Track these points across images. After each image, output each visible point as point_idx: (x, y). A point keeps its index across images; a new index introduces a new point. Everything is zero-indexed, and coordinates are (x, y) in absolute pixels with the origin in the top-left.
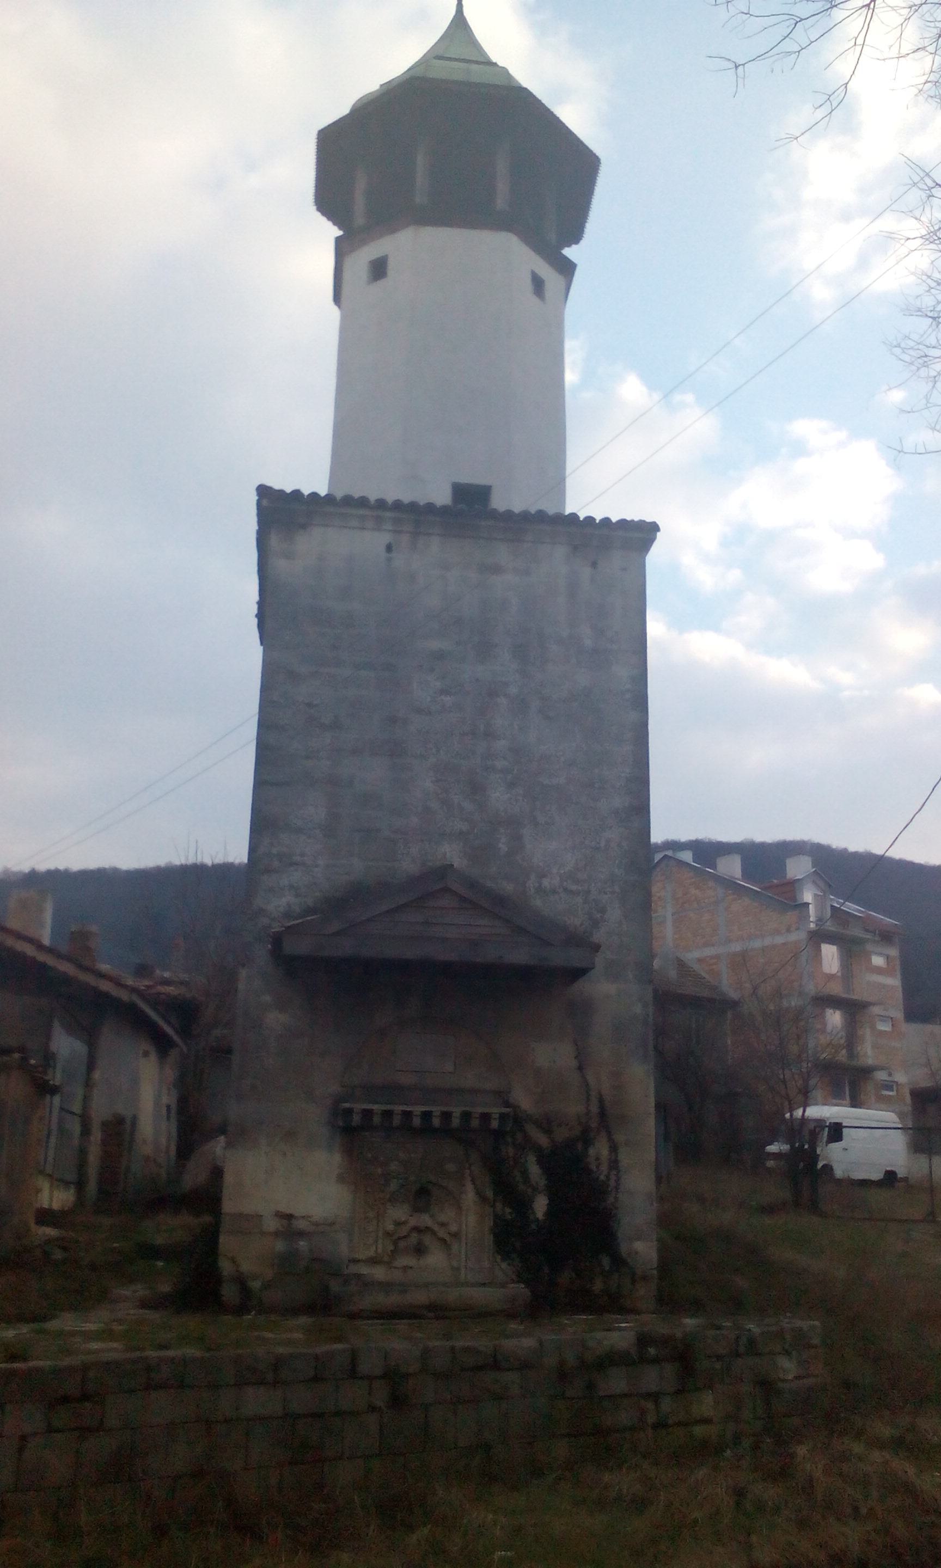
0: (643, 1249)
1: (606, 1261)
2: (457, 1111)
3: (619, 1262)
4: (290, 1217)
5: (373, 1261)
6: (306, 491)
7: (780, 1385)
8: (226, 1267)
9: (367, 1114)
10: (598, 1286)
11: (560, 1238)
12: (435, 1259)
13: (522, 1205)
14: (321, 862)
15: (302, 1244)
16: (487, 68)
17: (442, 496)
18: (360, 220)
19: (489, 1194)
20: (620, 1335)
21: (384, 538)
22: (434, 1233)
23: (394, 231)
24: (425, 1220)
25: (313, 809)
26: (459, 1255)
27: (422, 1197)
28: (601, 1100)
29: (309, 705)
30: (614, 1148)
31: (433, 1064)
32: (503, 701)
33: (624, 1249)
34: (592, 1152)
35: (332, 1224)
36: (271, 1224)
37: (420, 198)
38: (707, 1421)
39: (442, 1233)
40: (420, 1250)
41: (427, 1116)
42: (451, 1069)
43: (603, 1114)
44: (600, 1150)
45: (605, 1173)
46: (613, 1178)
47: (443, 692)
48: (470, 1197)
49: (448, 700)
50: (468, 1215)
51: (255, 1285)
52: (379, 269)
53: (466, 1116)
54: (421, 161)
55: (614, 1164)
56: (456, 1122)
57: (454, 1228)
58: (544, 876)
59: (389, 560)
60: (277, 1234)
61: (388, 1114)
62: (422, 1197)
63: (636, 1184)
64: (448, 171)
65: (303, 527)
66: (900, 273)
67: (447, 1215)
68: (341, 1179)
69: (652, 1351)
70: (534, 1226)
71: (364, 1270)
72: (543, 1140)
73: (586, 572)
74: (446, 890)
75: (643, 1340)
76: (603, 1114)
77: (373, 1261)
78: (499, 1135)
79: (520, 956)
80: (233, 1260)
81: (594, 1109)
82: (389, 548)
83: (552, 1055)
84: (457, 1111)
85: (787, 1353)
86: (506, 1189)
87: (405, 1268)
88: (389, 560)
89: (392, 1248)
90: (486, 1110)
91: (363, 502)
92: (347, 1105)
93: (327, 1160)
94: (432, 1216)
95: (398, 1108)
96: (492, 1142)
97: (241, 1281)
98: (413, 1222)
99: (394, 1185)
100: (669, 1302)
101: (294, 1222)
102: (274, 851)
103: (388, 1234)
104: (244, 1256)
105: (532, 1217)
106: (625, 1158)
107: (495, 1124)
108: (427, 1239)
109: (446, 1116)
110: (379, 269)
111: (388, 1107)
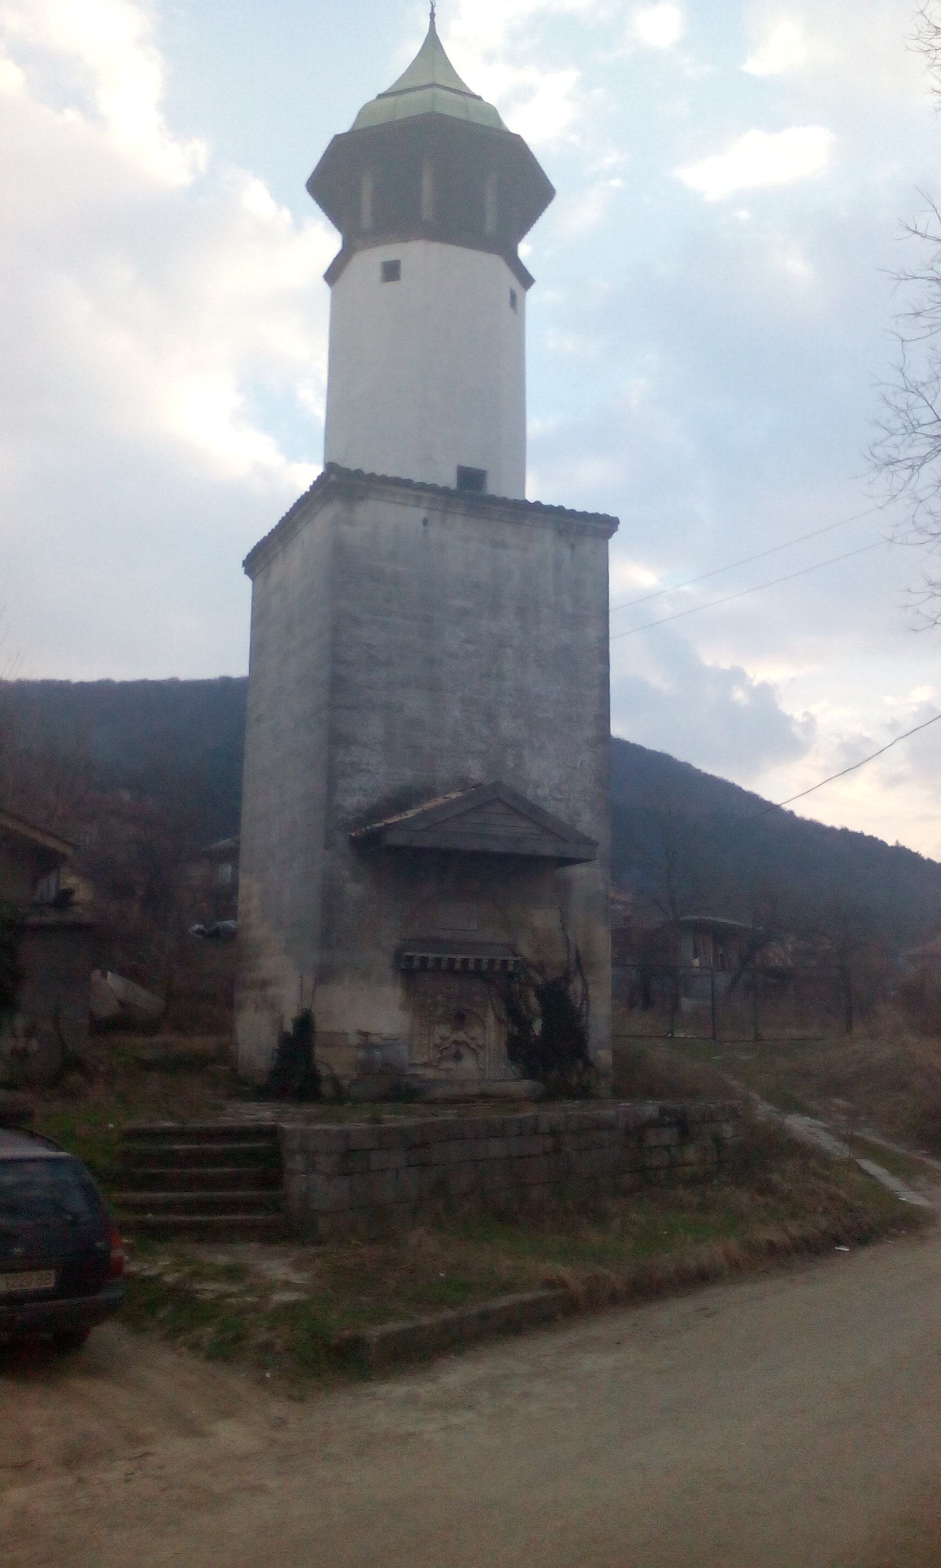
0: (603, 1056)
1: (580, 1064)
2: (485, 959)
3: (588, 1064)
4: (366, 1034)
5: (425, 1065)
6: (568, 508)
7: (725, 1141)
8: (324, 1071)
9: (424, 960)
10: (574, 1080)
11: (551, 1046)
12: (468, 1063)
13: (523, 1023)
14: (381, 770)
15: (377, 1053)
16: (459, 98)
17: (448, 479)
18: (367, 222)
19: (504, 1017)
20: (650, 1109)
21: (422, 513)
22: (468, 1046)
23: (406, 240)
24: (461, 1036)
25: (374, 729)
26: (482, 1060)
27: (460, 1019)
28: (577, 952)
29: (370, 646)
30: (586, 985)
31: (464, 924)
32: (509, 651)
33: (591, 1057)
34: (571, 988)
35: (396, 1039)
36: (354, 1040)
37: (427, 213)
38: (690, 1164)
39: (473, 1045)
40: (458, 1057)
41: (465, 962)
42: (475, 927)
43: (578, 959)
44: (576, 986)
45: (580, 1002)
46: (584, 1007)
47: (467, 641)
48: (491, 1019)
49: (470, 647)
50: (490, 1034)
51: (345, 1082)
52: (391, 271)
53: (492, 962)
54: (427, 183)
55: (586, 996)
56: (484, 967)
57: (481, 1042)
58: (539, 787)
59: (426, 531)
60: (358, 1046)
61: (438, 961)
62: (460, 1019)
63: (601, 1011)
64: (427, 185)
65: (361, 499)
66: (200, 149)
67: (477, 1031)
68: (403, 1007)
69: (667, 1119)
70: (533, 1039)
71: (420, 1071)
72: (539, 980)
73: (566, 552)
74: (499, 800)
75: (663, 1111)
76: (578, 959)
77: (425, 1065)
78: (511, 975)
79: (548, 849)
80: (328, 1065)
81: (573, 958)
82: (425, 522)
83: (544, 919)
84: (485, 959)
85: (727, 1121)
86: (515, 1015)
87: (448, 1070)
88: (426, 531)
89: (439, 1055)
90: (505, 958)
91: (407, 484)
92: (409, 954)
93: (393, 993)
94: (466, 1033)
95: (431, 956)
96: (503, 980)
97: (335, 1080)
98: (454, 1037)
99: (440, 1012)
100: (619, 1093)
101: (370, 1037)
102: (348, 760)
103: (436, 1046)
104: (334, 1062)
105: (532, 1034)
106: (593, 992)
107: (510, 968)
108: (463, 1050)
109: (478, 962)
110: (391, 271)
111: (439, 956)
